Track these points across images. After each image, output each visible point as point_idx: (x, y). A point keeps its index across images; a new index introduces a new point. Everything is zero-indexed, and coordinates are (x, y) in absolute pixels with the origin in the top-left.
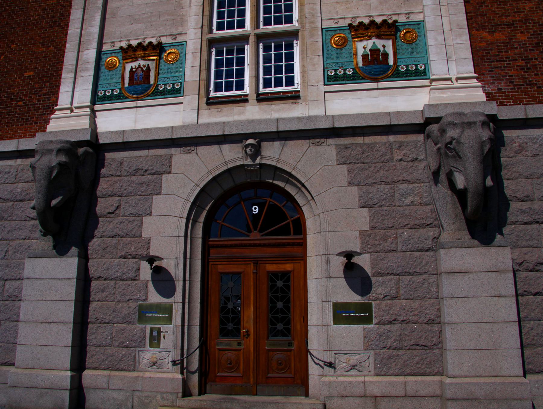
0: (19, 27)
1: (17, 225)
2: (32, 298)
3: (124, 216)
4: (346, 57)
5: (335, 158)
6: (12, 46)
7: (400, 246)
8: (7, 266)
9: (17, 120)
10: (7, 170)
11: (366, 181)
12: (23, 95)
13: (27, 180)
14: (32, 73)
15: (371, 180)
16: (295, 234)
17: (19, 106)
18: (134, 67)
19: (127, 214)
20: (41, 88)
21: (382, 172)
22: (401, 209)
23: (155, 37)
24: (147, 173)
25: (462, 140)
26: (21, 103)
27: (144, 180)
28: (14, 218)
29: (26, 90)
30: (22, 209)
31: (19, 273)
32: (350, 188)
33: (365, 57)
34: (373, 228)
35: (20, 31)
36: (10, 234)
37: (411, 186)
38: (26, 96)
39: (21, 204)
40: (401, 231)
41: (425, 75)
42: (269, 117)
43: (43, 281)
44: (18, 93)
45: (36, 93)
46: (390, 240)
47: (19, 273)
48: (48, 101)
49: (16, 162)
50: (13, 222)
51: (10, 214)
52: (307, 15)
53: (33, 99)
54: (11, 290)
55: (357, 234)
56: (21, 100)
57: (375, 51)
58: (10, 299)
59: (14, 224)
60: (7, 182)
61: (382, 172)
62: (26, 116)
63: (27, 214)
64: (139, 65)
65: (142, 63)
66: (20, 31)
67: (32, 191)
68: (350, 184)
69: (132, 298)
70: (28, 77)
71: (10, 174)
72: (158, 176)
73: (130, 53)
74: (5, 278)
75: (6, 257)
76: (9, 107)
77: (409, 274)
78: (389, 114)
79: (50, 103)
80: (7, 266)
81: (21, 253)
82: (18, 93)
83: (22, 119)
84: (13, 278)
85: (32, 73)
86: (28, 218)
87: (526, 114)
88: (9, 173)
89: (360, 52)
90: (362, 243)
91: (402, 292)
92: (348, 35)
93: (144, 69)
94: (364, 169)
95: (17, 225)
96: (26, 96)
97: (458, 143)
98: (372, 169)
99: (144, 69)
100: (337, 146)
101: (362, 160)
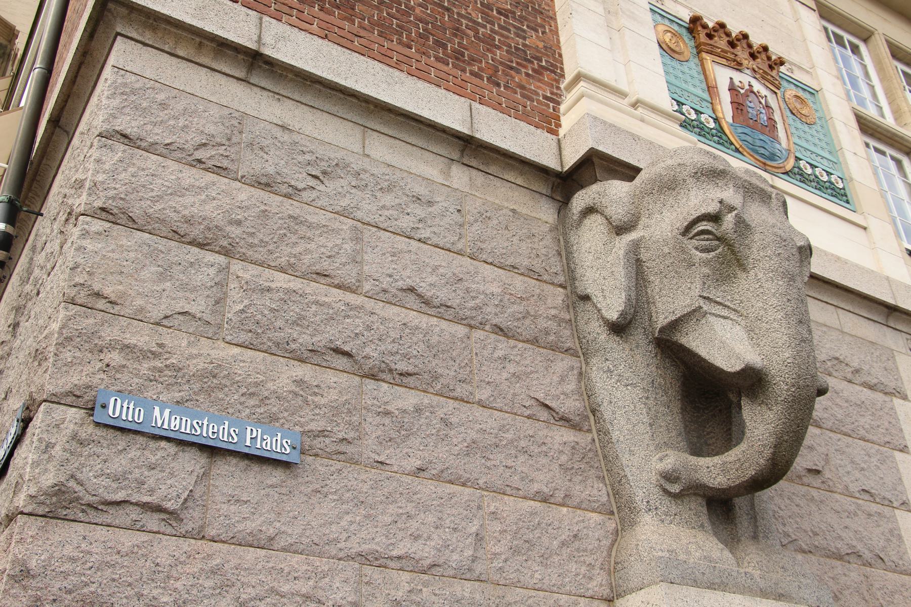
10: (421, 190)
18: (737, 83)
19: (854, 488)
28: (483, 394)
39: (503, 346)
51: (464, 374)
59: (490, 420)
60: (424, 234)
63: (541, 396)
79: (524, 45)
86: (544, 415)
88: (430, 203)
95: (502, 428)
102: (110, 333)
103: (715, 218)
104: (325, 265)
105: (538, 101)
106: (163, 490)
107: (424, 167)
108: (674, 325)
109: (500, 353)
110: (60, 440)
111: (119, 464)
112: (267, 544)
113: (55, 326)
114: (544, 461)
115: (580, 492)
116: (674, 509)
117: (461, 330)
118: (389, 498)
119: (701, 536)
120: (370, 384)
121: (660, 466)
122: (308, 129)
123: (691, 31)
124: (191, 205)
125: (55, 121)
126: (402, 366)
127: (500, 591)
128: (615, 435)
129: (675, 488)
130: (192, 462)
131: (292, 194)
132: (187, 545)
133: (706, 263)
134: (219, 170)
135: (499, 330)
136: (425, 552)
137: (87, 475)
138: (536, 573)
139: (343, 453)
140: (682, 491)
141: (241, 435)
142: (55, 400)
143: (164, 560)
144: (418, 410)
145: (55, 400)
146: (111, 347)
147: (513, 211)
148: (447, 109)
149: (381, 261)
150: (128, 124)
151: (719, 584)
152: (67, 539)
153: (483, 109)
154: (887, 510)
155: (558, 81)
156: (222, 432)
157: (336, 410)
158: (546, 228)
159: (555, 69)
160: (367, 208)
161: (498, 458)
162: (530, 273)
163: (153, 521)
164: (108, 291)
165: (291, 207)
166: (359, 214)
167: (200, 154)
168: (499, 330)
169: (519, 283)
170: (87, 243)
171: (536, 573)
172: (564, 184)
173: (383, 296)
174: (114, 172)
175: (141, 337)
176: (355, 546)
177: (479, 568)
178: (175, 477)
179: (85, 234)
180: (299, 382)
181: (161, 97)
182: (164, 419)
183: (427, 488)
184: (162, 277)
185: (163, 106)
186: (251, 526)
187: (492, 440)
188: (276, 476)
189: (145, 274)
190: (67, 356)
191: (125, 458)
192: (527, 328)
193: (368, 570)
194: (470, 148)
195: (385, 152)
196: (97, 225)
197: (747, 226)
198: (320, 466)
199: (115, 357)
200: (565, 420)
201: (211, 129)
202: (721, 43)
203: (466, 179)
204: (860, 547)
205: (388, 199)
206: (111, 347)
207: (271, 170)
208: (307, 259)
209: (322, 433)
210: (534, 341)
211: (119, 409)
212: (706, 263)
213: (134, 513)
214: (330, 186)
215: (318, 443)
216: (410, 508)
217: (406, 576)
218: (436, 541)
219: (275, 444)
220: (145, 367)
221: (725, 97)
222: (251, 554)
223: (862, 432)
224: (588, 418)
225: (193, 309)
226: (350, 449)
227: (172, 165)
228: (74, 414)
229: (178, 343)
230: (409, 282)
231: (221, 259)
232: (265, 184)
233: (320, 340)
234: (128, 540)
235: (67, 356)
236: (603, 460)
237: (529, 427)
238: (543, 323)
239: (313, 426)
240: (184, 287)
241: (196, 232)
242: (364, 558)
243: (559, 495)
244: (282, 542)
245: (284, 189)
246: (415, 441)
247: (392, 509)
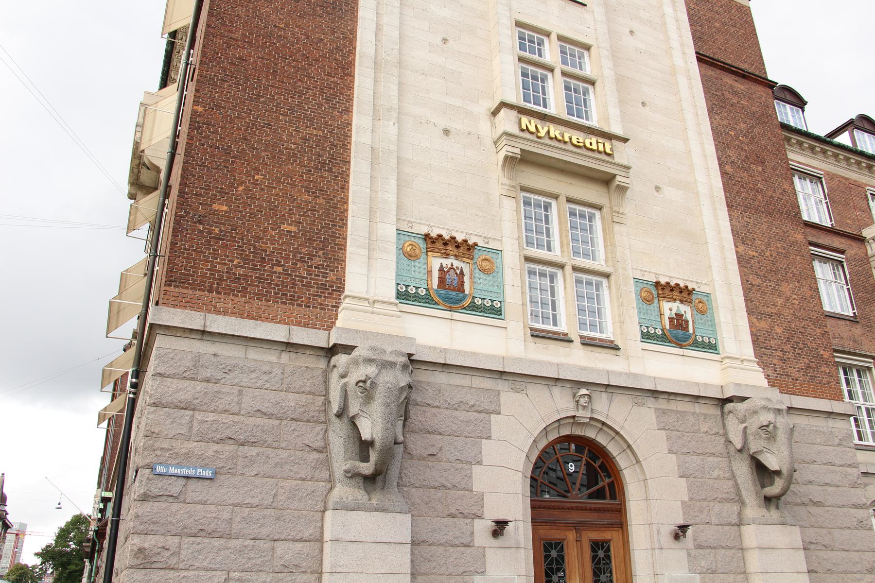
0: (266, 151)
1: (290, 456)
2: (346, 570)
3: (448, 461)
4: (419, 273)
5: (655, 423)
6: (256, 177)
7: (713, 519)
8: (278, 519)
9: (275, 293)
10: (266, 368)
11: (682, 450)
12: (282, 258)
13: (302, 390)
14: (293, 228)
15: (685, 450)
16: (611, 499)
17: (276, 272)
18: (444, 265)
19: (452, 459)
20: (311, 256)
21: (693, 443)
22: (711, 482)
23: (463, 232)
24: (473, 409)
25: (778, 425)
26: (279, 269)
27: (471, 418)
28: (283, 445)
29: (285, 250)
30: (296, 433)
31: (300, 531)
32: (670, 455)
33: (671, 320)
34: (691, 499)
35: (268, 158)
36: (279, 469)
37: (716, 459)
38: (286, 259)
39: (294, 425)
40: (712, 504)
41: (501, 315)
42: (593, 365)
43: (361, 545)
44: (273, 252)
45: (302, 260)
46: (705, 513)
47: (300, 531)
48: (323, 277)
49: (279, 358)
50: (281, 452)
51: (276, 439)
52: (619, 259)
53: (299, 269)
54: (287, 557)
55: (679, 503)
56: (278, 264)
57: (679, 316)
58: (286, 570)
59: (284, 454)
60: (266, 387)
61: (693, 443)
62: (289, 291)
63: (307, 442)
64: (452, 265)
65: (457, 264)
66: (268, 158)
67: (312, 408)
68: (670, 451)
69: (467, 569)
70: (288, 231)
71: (272, 375)
72: (487, 416)
73: (667, 291)
74: (276, 538)
75: (274, 505)
76: (260, 270)
77: (723, 548)
78: (697, 384)
79: (326, 281)
80: (278, 519)
81: (299, 500)
82: (273, 252)
83: (283, 294)
84: (290, 537)
85: (293, 228)
86: (308, 449)
87: (205, 326)
88: (270, 373)
89: (667, 314)
90: (684, 514)
91: (719, 566)
92: (422, 245)
93: (458, 272)
94: (679, 438)
95: (290, 456)
96: (286, 259)
97: (775, 427)
98: (685, 438)
99: (458, 272)
100: (656, 409)
101: (677, 428)
102: (157, 445)
103: (364, 382)
104: (227, 407)
105: (329, 310)
106: (173, 491)
107: (270, 357)
108: (353, 417)
109: (292, 428)
110: (144, 479)
111: (160, 485)
112: (204, 503)
113: (142, 444)
114: (305, 466)
115: (317, 475)
116: (348, 482)
117: (277, 422)
118: (245, 486)
119: (357, 490)
120: (241, 447)
121: (344, 468)
122: (225, 353)
123: (425, 240)
124: (181, 396)
125: (147, 344)
126: (252, 440)
127: (281, 511)
128: (333, 455)
129: (349, 475)
130: (182, 481)
131: (217, 382)
132: (180, 505)
133: (362, 397)
134: (191, 379)
135: (292, 419)
136: (256, 501)
137: (152, 489)
138: (296, 504)
139: (231, 473)
140: (353, 475)
141: (196, 472)
142: (143, 467)
143: (174, 511)
144: (257, 454)
145: (143, 467)
146: (157, 449)
147: (307, 367)
148: (278, 332)
149: (247, 403)
150: (161, 370)
151: (356, 508)
152: (148, 506)
153: (295, 328)
154: (467, 467)
155: (340, 296)
156: (191, 472)
157: (227, 459)
158: (320, 372)
159: (340, 290)
160: (245, 381)
161: (286, 467)
162: (310, 393)
163: (171, 499)
164: (156, 431)
165: (216, 387)
166: (242, 384)
167: (185, 375)
168: (292, 419)
169: (304, 398)
170: (149, 416)
171: (296, 504)
172: (332, 351)
173: (249, 415)
174: (157, 389)
175: (166, 445)
176: (232, 502)
177: (274, 505)
178: (176, 487)
179: (149, 413)
180: (216, 452)
181: (171, 356)
182: (173, 470)
183: (258, 481)
184: (173, 422)
185: (172, 359)
186: (199, 498)
187: (284, 461)
188: (208, 482)
189: (167, 423)
190: (145, 454)
191: (161, 483)
192: (305, 416)
193: (235, 508)
194: (289, 346)
195: (255, 354)
196: (153, 409)
197: (376, 384)
198: (222, 477)
199: (159, 452)
200: (316, 450)
201: (188, 364)
202: (439, 245)
203: (287, 357)
204: (446, 483)
205: (254, 375)
206: (157, 449)
207: (209, 375)
208: (221, 406)
209: (223, 467)
210: (308, 421)
211: (160, 469)
212: (362, 397)
213: (165, 498)
214: (232, 375)
215: (222, 470)
216: (252, 488)
217: (248, 509)
218: (259, 498)
219: (208, 473)
220: (167, 454)
221: (436, 275)
222: (199, 507)
223: (466, 434)
224: (324, 449)
225: (182, 432)
226: (232, 471)
227: (175, 381)
228: (148, 471)
229: (177, 444)
230: (258, 408)
231: (191, 413)
232: (207, 380)
233: (224, 436)
234: (164, 505)
235: (145, 454)
236: (327, 463)
237: (300, 454)
238: (311, 414)
239: (220, 465)
240: (179, 424)
241: (183, 405)
242: (234, 505)
243: (309, 478)
244: (209, 502)
245: (214, 381)
246: (255, 465)
247: (245, 489)
